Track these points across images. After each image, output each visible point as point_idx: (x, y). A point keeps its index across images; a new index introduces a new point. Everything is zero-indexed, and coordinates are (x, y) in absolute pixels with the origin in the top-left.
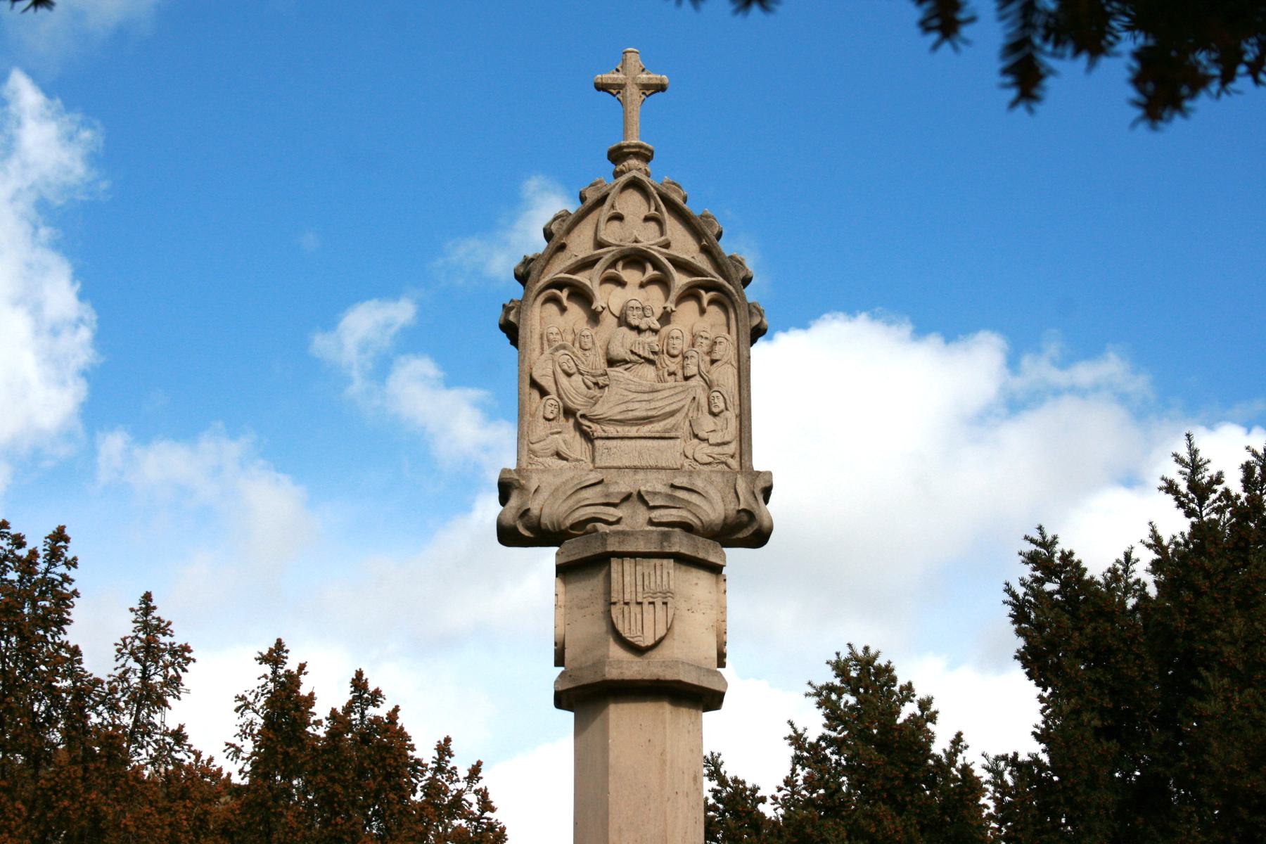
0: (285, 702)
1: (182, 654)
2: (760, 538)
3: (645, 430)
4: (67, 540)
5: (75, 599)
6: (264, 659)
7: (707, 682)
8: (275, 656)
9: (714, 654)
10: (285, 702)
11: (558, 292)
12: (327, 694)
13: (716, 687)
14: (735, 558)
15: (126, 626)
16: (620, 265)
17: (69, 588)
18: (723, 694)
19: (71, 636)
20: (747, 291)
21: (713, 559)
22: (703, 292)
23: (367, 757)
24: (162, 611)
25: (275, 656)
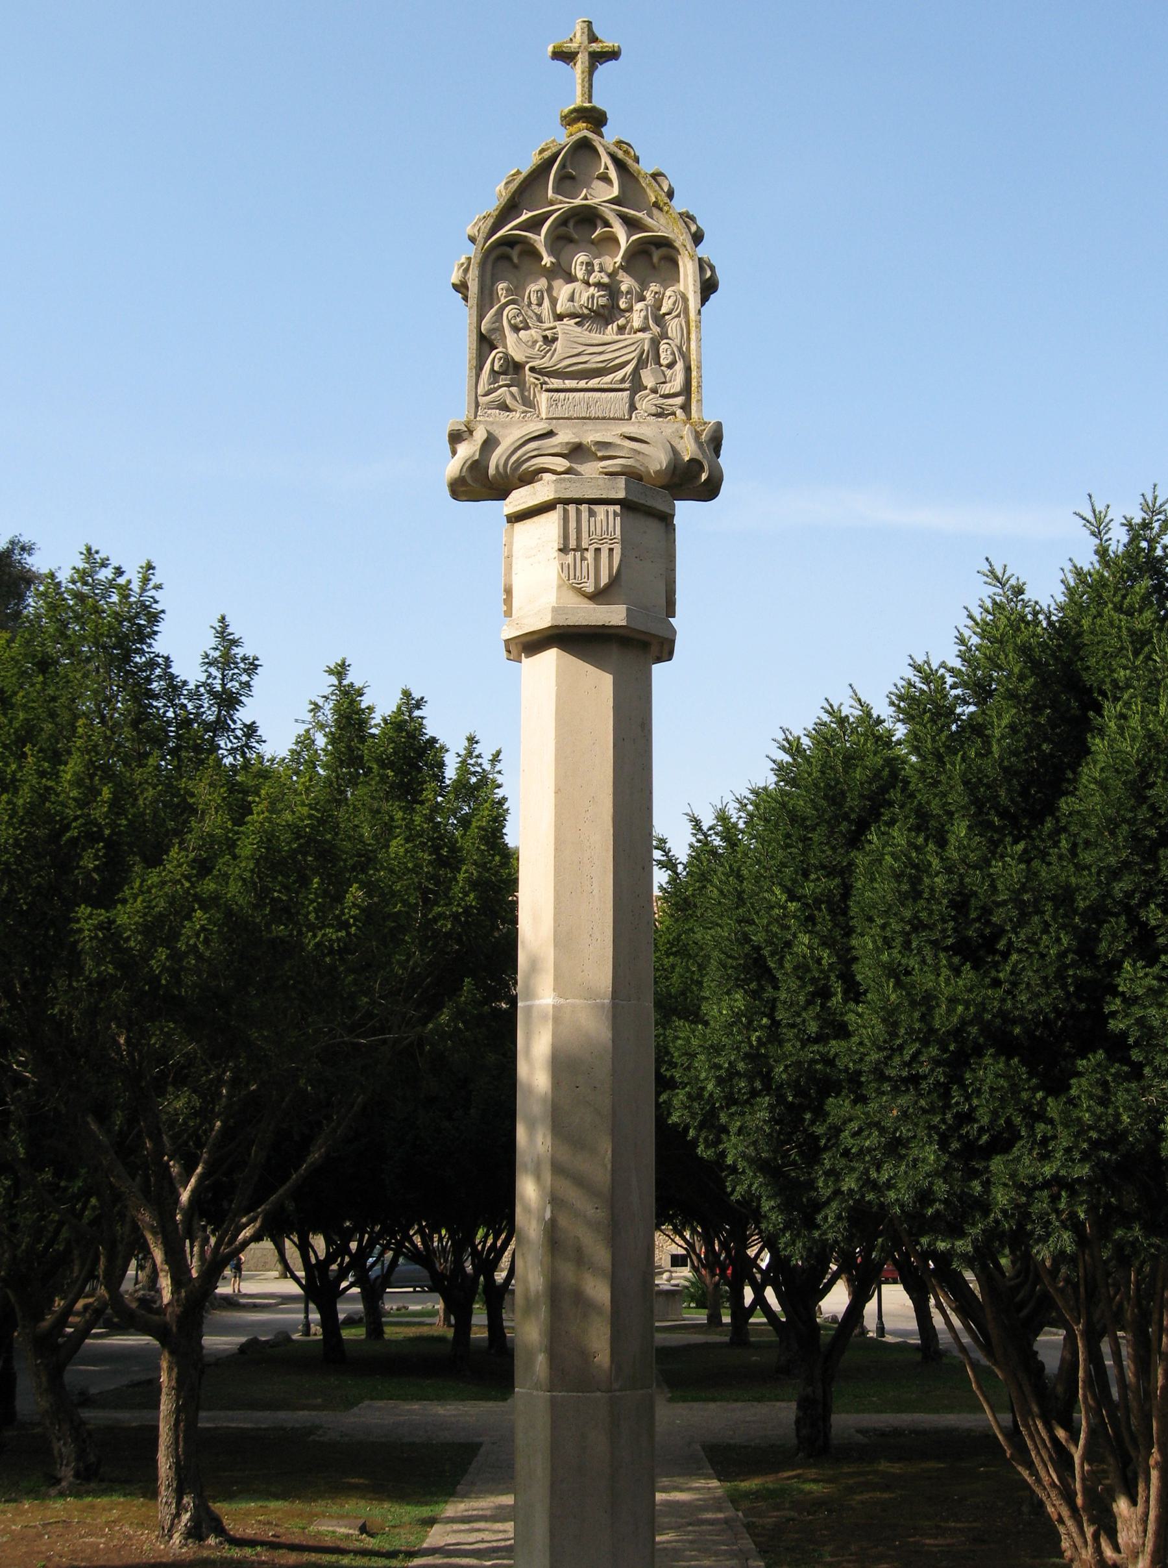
0: (349, 713)
1: (252, 667)
2: (710, 490)
3: (593, 383)
4: (154, 568)
5: (162, 615)
6: (330, 672)
7: (655, 629)
8: (340, 671)
9: (663, 602)
10: (349, 713)
11: (508, 249)
12: (381, 704)
13: (666, 634)
14: (686, 512)
15: (209, 642)
16: (571, 224)
17: (159, 607)
18: (674, 641)
19: (160, 645)
20: (674, 203)
21: (660, 506)
22: (653, 248)
23: (404, 755)
24: (236, 629)
25: (340, 671)
